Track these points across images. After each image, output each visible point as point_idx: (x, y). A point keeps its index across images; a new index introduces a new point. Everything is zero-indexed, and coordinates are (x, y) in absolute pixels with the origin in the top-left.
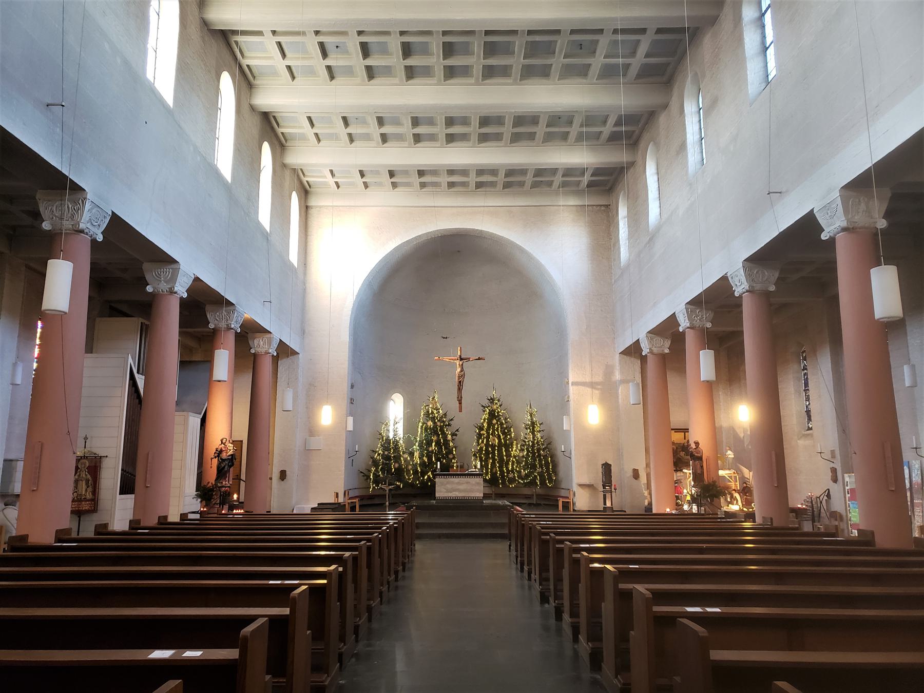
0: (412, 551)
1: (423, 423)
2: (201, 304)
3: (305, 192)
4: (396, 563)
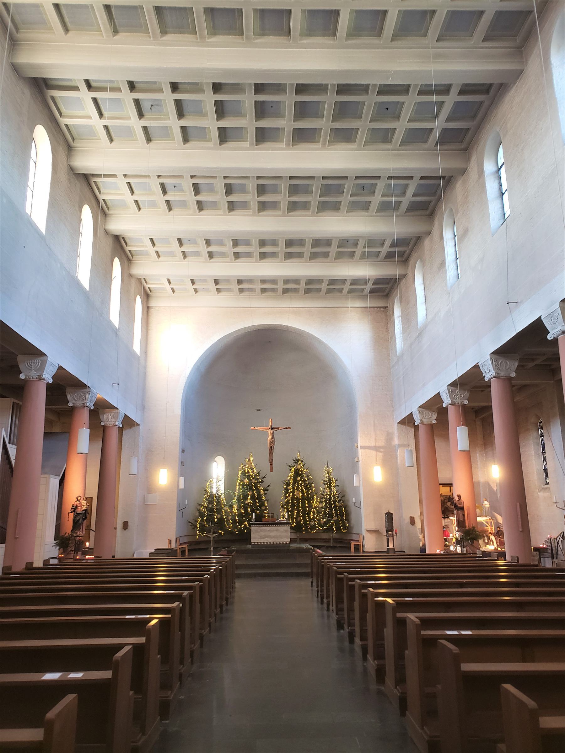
0: (233, 588)
1: (241, 481)
2: (63, 387)
3: (147, 295)
4: (221, 598)
